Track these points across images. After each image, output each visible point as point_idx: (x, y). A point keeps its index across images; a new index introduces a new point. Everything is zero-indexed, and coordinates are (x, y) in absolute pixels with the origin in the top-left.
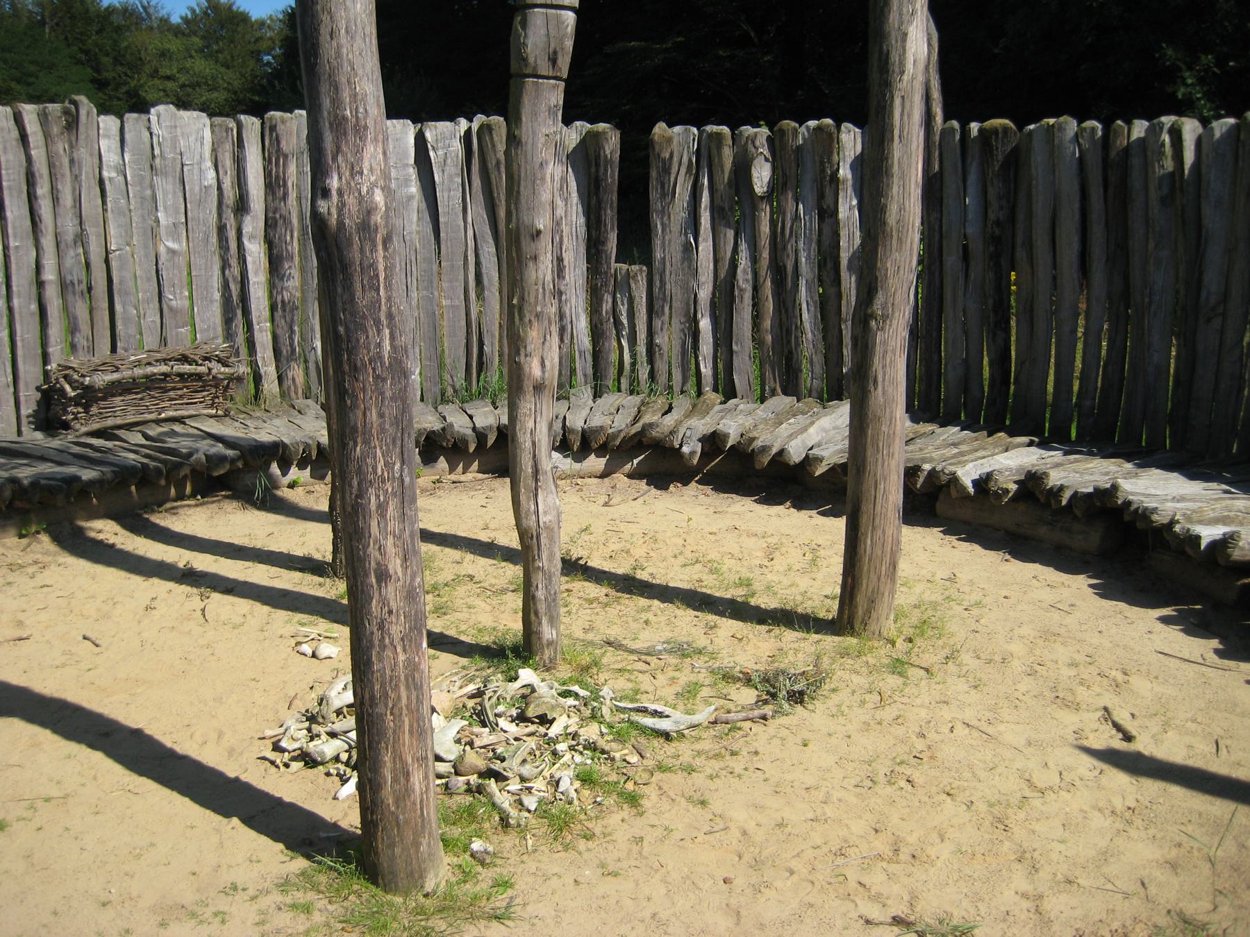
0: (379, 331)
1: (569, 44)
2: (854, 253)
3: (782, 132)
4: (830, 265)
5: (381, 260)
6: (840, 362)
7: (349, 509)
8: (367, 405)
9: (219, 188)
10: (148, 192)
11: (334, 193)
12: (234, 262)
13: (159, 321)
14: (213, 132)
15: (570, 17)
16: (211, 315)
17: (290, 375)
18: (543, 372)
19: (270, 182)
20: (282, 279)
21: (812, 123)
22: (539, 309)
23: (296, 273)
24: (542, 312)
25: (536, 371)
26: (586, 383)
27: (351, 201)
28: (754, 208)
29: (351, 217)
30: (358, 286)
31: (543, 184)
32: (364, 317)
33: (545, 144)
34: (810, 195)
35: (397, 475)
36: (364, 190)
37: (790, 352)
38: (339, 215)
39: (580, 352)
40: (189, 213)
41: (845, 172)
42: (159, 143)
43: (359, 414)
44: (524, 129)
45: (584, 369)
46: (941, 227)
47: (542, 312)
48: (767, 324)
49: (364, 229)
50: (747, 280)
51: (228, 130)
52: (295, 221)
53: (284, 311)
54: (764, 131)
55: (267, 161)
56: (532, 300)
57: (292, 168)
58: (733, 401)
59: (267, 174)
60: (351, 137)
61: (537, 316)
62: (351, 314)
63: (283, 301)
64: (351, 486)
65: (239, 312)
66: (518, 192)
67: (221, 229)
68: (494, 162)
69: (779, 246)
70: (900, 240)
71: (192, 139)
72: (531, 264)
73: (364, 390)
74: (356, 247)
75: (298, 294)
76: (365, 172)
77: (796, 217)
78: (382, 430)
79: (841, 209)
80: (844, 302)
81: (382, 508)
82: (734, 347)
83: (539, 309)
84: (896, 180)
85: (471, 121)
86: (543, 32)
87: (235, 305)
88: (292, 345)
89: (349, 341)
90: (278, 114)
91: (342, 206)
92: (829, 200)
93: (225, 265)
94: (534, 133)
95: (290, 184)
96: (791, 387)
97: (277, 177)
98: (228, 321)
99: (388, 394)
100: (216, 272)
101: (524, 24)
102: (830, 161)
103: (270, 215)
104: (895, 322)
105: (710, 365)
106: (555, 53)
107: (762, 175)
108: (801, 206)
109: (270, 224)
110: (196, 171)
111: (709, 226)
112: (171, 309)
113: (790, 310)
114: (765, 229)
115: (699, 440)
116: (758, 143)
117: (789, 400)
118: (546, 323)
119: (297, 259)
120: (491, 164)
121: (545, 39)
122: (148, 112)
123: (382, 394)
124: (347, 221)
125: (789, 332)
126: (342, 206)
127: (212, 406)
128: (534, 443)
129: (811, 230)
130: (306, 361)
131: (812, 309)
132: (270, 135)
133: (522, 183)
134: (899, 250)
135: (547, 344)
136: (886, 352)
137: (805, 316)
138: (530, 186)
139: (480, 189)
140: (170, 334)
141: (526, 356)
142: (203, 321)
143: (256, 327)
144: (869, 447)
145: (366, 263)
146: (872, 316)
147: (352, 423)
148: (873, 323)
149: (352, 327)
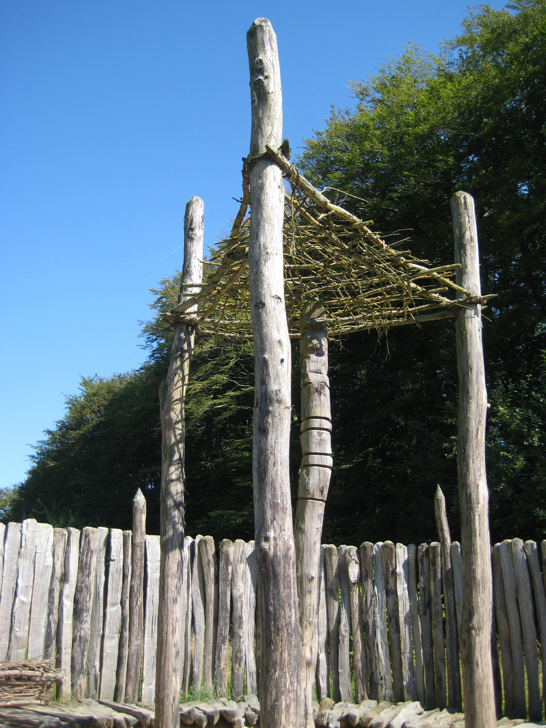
0: (290, 610)
1: (328, 484)
2: (407, 614)
3: (365, 548)
4: (393, 621)
5: (292, 573)
6: (401, 678)
7: (270, 708)
8: (283, 649)
9: (54, 568)
10: (15, 567)
11: (272, 539)
12: (55, 611)
13: (7, 644)
14: (54, 536)
15: (329, 472)
16: (37, 644)
17: (79, 682)
18: (311, 655)
19: (82, 566)
20: (81, 623)
21: (380, 544)
22: (311, 620)
23: (89, 619)
24: (312, 621)
25: (308, 655)
26: (253, 693)
27: (280, 543)
28: (350, 590)
29: (280, 551)
30: (282, 586)
31: (315, 553)
32: (284, 602)
33: (316, 533)
34: (380, 582)
35: (295, 689)
36: (286, 539)
37: (372, 673)
38: (275, 550)
39: (250, 673)
40: (35, 581)
41: (400, 569)
42: (26, 539)
43: (278, 654)
44: (306, 525)
45: (252, 684)
46: (454, 599)
47: (312, 621)
48: (359, 656)
49: (286, 557)
50: (346, 631)
51: (63, 535)
52: (92, 589)
53: (80, 642)
54: (354, 549)
55: (81, 554)
56: (308, 614)
57: (94, 559)
58: (340, 703)
59: (80, 561)
60: (280, 513)
61: (310, 623)
62: (277, 600)
63: (80, 636)
64: (271, 694)
65: (54, 642)
66: (303, 557)
67: (51, 591)
68: (206, 561)
69: (364, 611)
70: (483, 587)
71: (43, 539)
72: (308, 595)
73: (282, 641)
74: (282, 566)
75: (89, 632)
76: (286, 530)
77: (374, 595)
78: (290, 663)
79: (398, 590)
80: (402, 643)
81: (288, 707)
82: (340, 671)
83: (311, 620)
84: (479, 556)
85: (194, 538)
86: (317, 477)
87: (53, 638)
88: (82, 664)
89: (275, 614)
90: (90, 528)
91: (276, 545)
92: (391, 585)
93: (50, 612)
94: (311, 527)
95: (92, 568)
96: (373, 695)
97: (86, 563)
98: (47, 647)
99: (293, 643)
100: (45, 616)
101: (308, 474)
102: (391, 563)
103: (79, 584)
104: (484, 631)
105: (325, 681)
106: (323, 488)
107: (354, 571)
108: (376, 588)
109: (79, 590)
110: (42, 557)
111: (324, 600)
112: (16, 637)
113: (372, 647)
114: (356, 601)
115: (339, 720)
116: (351, 554)
117: (374, 703)
118: (313, 627)
119: (91, 611)
120: (205, 563)
121: (318, 481)
122: (21, 522)
123: (291, 643)
124: (278, 553)
125: (371, 661)
126: (276, 545)
127: (38, 699)
128: (305, 696)
129: (382, 601)
130: (88, 674)
131: (384, 647)
132: (84, 539)
133: (305, 552)
134: (484, 592)
135: (313, 639)
136: (481, 648)
137: (380, 651)
138: (309, 554)
139: (197, 576)
140: (13, 653)
141: (303, 645)
142: (33, 646)
143: (63, 651)
144: (477, 702)
145: (286, 575)
146: (473, 628)
147: (274, 659)
148: (473, 632)
149: (277, 607)
